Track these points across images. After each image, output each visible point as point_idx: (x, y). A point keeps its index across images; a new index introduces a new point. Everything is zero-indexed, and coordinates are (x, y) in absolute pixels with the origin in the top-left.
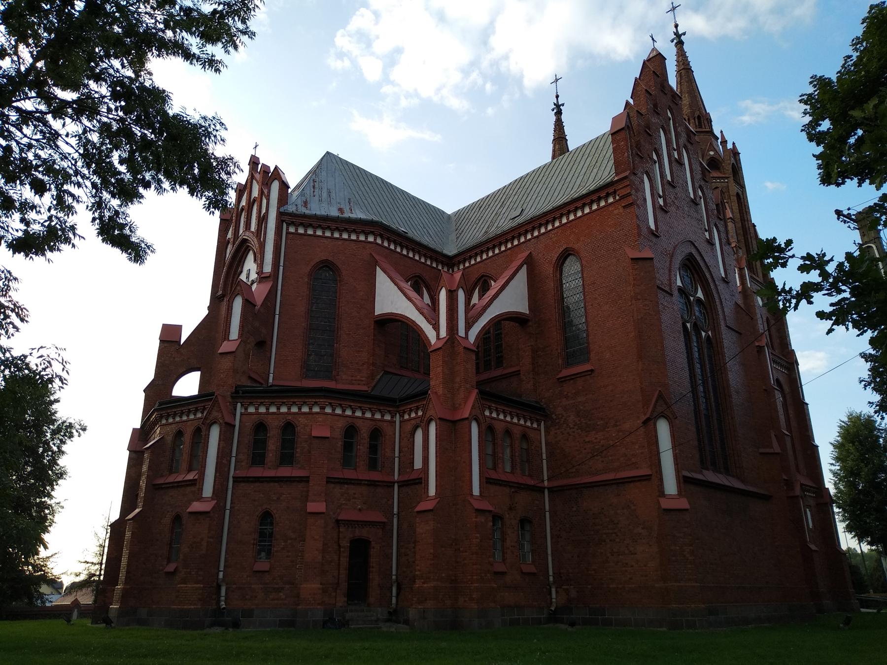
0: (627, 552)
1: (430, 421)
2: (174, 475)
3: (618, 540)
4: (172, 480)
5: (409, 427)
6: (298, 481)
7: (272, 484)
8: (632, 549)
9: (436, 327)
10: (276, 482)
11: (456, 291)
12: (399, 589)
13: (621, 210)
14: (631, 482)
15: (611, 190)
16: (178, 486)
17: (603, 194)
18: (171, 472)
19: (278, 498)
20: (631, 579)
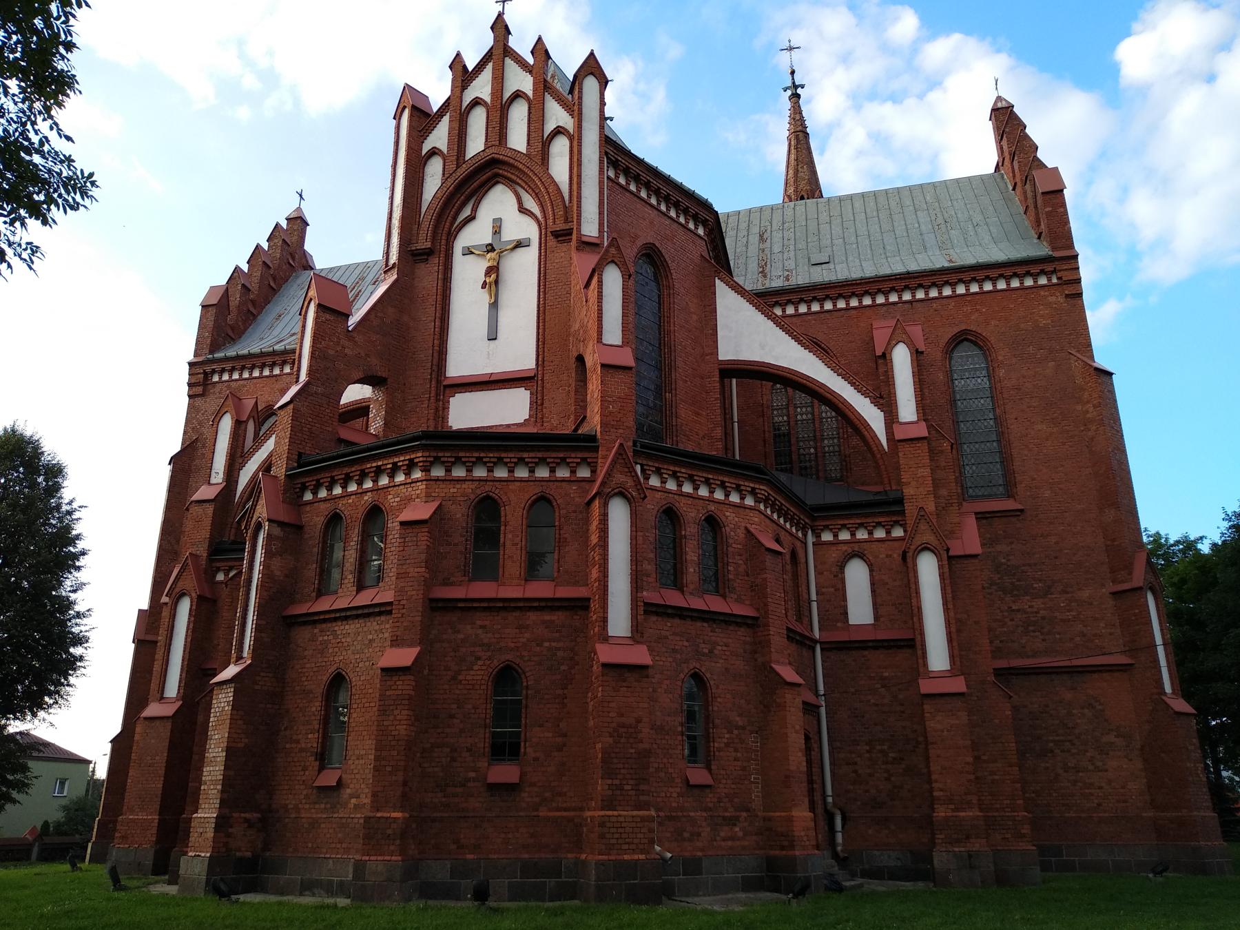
0: (1091, 767)
1: (182, 595)
2: (331, 598)
3: (1074, 751)
4: (326, 608)
5: (834, 555)
6: (737, 624)
7: (699, 624)
8: (1099, 764)
9: (885, 399)
10: (704, 620)
11: (246, 422)
12: (844, 819)
13: (1061, 299)
14: (1094, 672)
15: (1049, 268)
16: (504, 608)
17: (1034, 270)
18: (320, 594)
19: (711, 651)
20: (1099, 805)
